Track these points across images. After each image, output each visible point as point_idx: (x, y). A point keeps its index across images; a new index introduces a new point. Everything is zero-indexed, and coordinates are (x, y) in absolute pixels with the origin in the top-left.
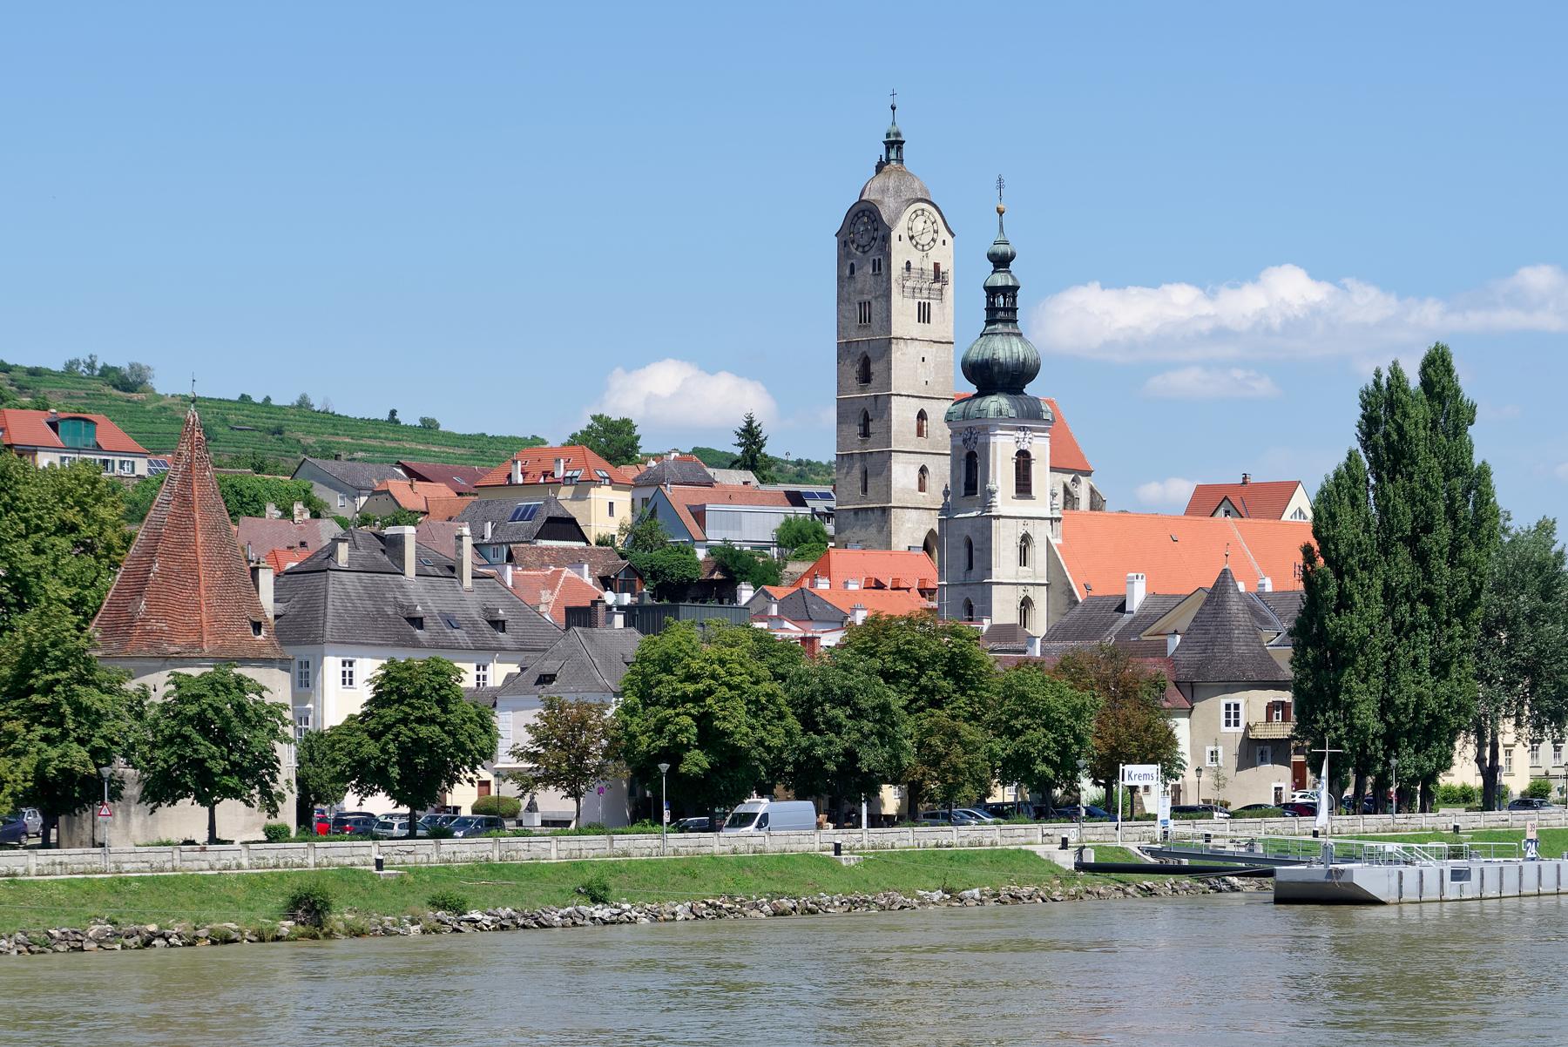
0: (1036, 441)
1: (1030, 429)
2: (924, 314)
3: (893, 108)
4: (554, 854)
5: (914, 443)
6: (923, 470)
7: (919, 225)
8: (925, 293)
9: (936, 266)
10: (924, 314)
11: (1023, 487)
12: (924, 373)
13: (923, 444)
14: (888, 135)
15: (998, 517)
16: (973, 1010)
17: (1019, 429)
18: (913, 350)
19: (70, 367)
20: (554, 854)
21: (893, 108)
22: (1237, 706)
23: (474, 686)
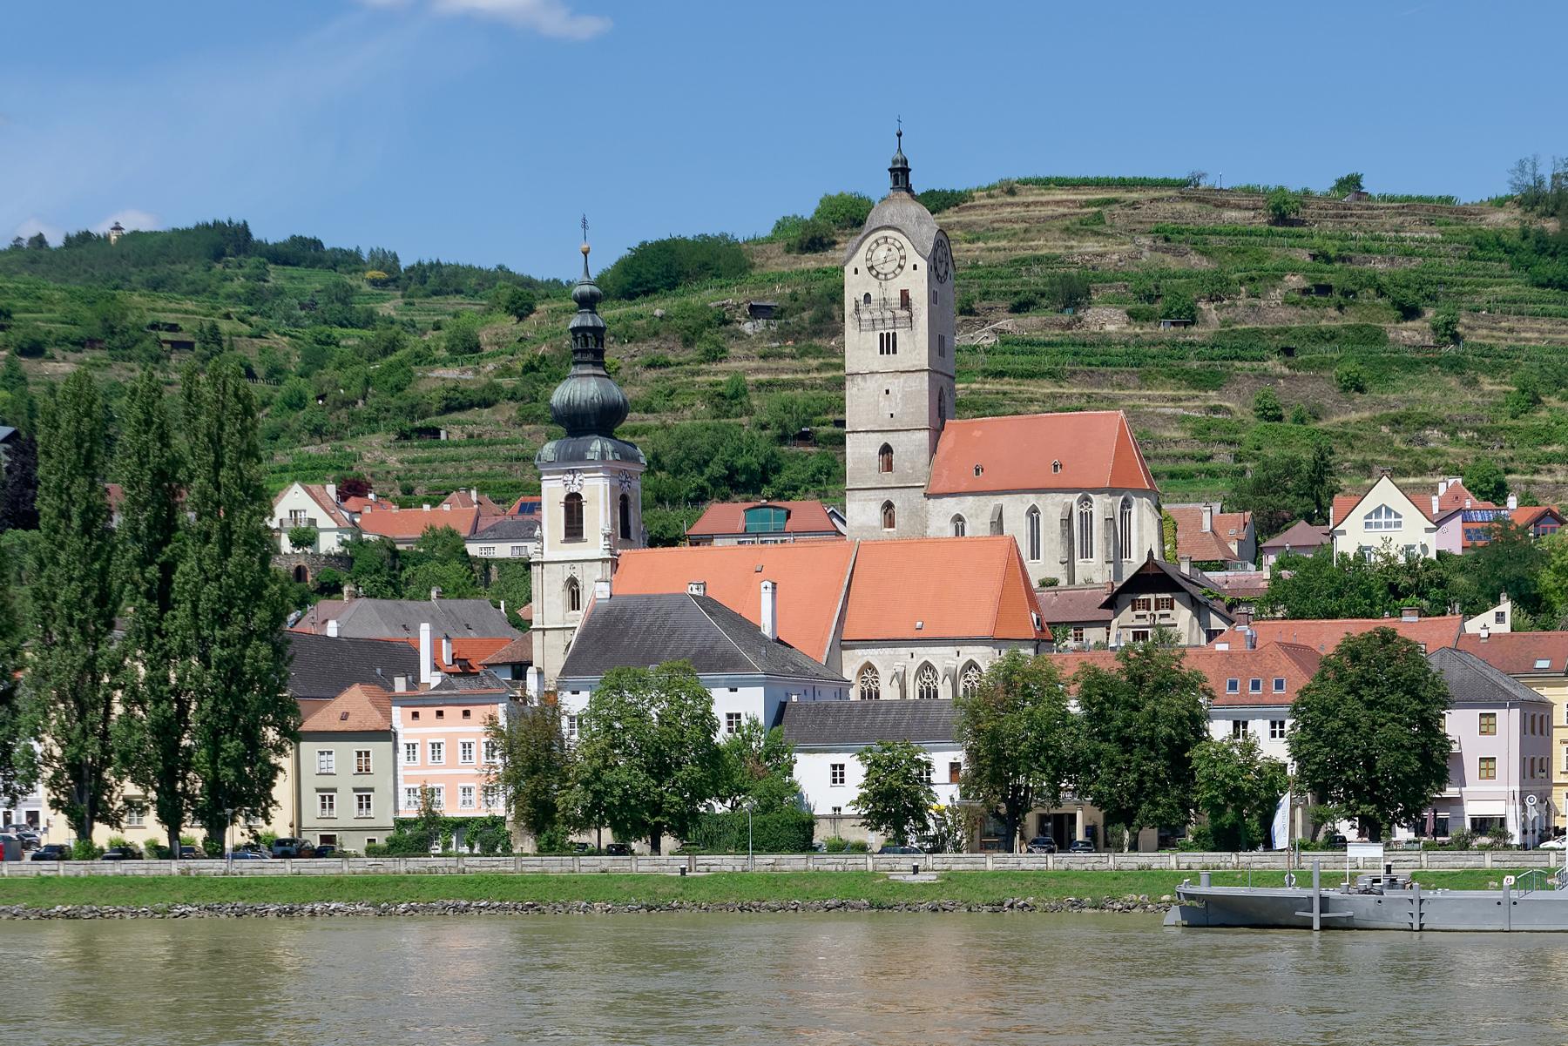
0: (587, 482)
1: (580, 471)
2: (888, 345)
3: (899, 135)
5: (874, 477)
6: (888, 506)
7: (881, 253)
9: (905, 295)
10: (888, 345)
11: (574, 529)
12: (886, 407)
13: (890, 479)
14: (895, 162)
15: (604, 560)
17: (568, 472)
18: (872, 384)
21: (899, 135)
22: (367, 754)
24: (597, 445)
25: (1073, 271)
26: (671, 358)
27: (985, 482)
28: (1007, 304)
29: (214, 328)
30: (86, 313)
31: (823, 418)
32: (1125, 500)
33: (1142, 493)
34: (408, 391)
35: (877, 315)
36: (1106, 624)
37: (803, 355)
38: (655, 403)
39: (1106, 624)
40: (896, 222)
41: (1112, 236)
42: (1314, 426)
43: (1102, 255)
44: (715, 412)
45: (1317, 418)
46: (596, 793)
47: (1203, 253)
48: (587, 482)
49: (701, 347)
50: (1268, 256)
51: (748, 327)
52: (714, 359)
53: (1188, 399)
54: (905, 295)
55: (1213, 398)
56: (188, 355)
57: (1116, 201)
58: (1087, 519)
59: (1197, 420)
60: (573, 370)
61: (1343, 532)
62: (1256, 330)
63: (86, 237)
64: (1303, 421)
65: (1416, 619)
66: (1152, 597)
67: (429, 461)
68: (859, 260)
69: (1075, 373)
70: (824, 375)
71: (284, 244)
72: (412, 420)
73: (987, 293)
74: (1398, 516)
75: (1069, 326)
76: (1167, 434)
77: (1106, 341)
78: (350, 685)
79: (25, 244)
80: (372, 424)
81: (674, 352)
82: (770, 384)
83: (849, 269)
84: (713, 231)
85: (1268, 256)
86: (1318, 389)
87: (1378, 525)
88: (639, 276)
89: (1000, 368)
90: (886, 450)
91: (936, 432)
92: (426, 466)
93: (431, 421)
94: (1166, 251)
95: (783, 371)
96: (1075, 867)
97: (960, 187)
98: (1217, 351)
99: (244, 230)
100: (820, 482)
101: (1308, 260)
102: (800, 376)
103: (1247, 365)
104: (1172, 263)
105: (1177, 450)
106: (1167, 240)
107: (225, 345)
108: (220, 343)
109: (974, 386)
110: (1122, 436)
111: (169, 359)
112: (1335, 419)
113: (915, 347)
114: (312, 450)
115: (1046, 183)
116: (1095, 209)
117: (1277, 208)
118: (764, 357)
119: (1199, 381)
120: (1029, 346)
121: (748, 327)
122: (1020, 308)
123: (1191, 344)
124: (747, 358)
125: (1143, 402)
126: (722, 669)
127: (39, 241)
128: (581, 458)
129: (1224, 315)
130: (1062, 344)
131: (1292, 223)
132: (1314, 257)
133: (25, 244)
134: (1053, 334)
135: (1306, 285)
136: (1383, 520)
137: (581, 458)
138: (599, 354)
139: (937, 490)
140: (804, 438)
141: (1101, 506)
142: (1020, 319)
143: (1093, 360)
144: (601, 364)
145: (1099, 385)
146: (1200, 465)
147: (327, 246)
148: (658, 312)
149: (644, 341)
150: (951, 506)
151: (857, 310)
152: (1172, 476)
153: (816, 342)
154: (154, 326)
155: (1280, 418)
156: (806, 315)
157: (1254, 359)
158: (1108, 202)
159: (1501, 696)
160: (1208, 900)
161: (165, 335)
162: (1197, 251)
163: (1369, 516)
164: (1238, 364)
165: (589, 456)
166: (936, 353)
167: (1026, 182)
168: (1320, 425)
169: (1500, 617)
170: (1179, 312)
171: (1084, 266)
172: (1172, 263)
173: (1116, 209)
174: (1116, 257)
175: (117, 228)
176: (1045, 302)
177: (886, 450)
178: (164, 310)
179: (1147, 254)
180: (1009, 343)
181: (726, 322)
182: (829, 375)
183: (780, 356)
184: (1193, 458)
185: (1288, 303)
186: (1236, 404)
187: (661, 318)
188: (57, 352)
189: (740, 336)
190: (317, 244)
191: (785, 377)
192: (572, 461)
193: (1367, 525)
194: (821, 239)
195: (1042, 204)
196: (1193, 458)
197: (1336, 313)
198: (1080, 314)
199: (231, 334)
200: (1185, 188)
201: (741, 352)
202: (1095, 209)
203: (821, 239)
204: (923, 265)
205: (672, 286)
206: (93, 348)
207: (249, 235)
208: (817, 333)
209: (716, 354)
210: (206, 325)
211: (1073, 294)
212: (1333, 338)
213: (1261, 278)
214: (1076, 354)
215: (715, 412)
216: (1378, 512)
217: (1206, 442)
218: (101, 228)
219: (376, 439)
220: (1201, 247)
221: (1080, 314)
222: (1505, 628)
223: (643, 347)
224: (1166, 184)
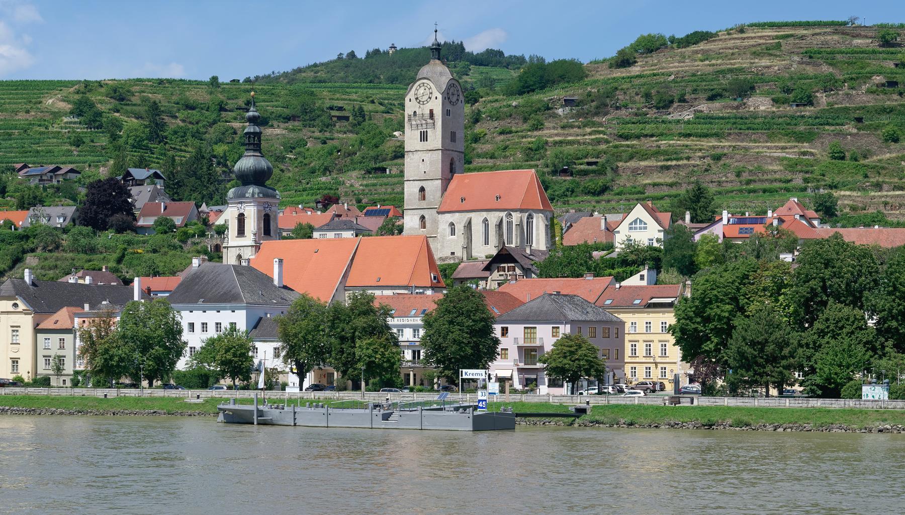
0: (247, 208)
2: (424, 137)
4: (787, 404)
6: (423, 218)
7: (421, 91)
8: (424, 126)
9: (431, 111)
10: (424, 137)
11: (241, 232)
13: (424, 204)
15: (252, 246)
16: (313, 462)
18: (417, 157)
19: (340, 58)
20: (787, 404)
23: (245, 311)
24: (251, 190)
25: (749, 77)
26: (514, 129)
27: (466, 205)
28: (706, 96)
29: (361, 110)
30: (295, 102)
31: (581, 161)
32: (530, 215)
33: (538, 211)
34: (381, 148)
35: (419, 122)
36: (486, 279)
37: (585, 126)
38: (496, 154)
39: (486, 279)
40: (429, 75)
41: (779, 56)
42: (862, 162)
43: (768, 67)
44: (526, 158)
45: (865, 157)
46: (106, 360)
47: (831, 64)
48: (247, 208)
49: (531, 122)
50: (869, 65)
51: (560, 111)
52: (536, 129)
53: (791, 148)
54: (431, 111)
55: (806, 147)
56: (346, 123)
57: (792, 36)
58: (510, 224)
59: (790, 159)
60: (246, 154)
61: (618, 232)
62: (846, 108)
63: (377, 52)
64: (856, 160)
65: (591, 278)
66: (506, 265)
67: (374, 185)
68: (411, 95)
69: (730, 134)
70: (593, 137)
71: (482, 54)
72: (376, 163)
73: (696, 90)
74: (645, 224)
75: (737, 108)
76: (771, 168)
77: (755, 116)
78: (62, 308)
79: (344, 56)
80: (353, 166)
81: (516, 125)
82: (561, 142)
83: (407, 99)
84: (568, 57)
85: (869, 65)
86: (868, 140)
87: (636, 228)
88: (526, 82)
89: (688, 132)
90: (422, 189)
91: (446, 182)
92: (372, 188)
93: (383, 164)
94: (808, 64)
95: (570, 135)
96: (273, 397)
97: (713, 31)
98: (817, 120)
99: (461, 47)
100: (566, 196)
101: (893, 66)
102: (579, 138)
103: (832, 128)
104: (810, 70)
105: (777, 176)
106: (811, 57)
107: (367, 118)
108: (364, 116)
109: (671, 142)
110: (531, 183)
111: (335, 125)
112: (875, 158)
113: (436, 138)
114: (323, 179)
115: (762, 26)
116: (777, 41)
117: (883, 37)
118: (563, 127)
119: (800, 138)
120: (710, 119)
121: (560, 111)
122: (711, 98)
123: (803, 117)
124: (554, 128)
125: (765, 150)
126: (230, 302)
127: (352, 55)
128: (243, 196)
129: (831, 100)
130: (729, 118)
131: (893, 45)
132: (897, 65)
133: (344, 56)
134: (725, 113)
135: (884, 81)
136: (638, 226)
137: (243, 196)
138: (259, 145)
139: (443, 210)
140: (564, 172)
141: (516, 217)
142: (717, 104)
143: (743, 127)
144: (259, 151)
145: (742, 141)
146: (783, 185)
147: (506, 55)
148: (514, 104)
149: (504, 119)
150: (449, 218)
151: (410, 120)
152: (765, 191)
153: (596, 119)
154: (331, 108)
155: (843, 158)
156: (594, 104)
157: (837, 124)
158: (788, 36)
159: (562, 318)
160: (235, 411)
161: (334, 113)
162: (827, 63)
163: (631, 224)
164: (827, 127)
165: (247, 195)
166: (448, 141)
167: (751, 25)
168: (866, 162)
169: (642, 278)
170: (801, 99)
171: (757, 74)
172: (810, 70)
173: (791, 40)
174: (776, 68)
175: (393, 47)
176: (727, 94)
177: (422, 189)
178: (337, 99)
179: (795, 66)
180: (701, 118)
181: (548, 109)
182: (593, 137)
183: (572, 127)
184: (780, 181)
185: (870, 92)
186: (818, 151)
187: (515, 107)
188: (275, 123)
189: (555, 116)
190: (501, 53)
191: (570, 138)
192: (240, 197)
193: (630, 228)
194: (628, 60)
195: (752, 38)
196: (780, 181)
197: (899, 97)
198: (745, 101)
199: (370, 112)
200: (838, 27)
201: (551, 125)
202: (777, 41)
203: (628, 60)
204: (440, 97)
205: (542, 88)
206: (294, 120)
207: (464, 49)
208: (597, 114)
209: (537, 127)
210: (357, 107)
211: (744, 89)
212: (891, 111)
213: (858, 78)
214: (735, 123)
215: (526, 158)
216: (635, 221)
217: (793, 172)
218: (384, 47)
219: (354, 174)
220: (829, 61)
221: (745, 101)
222: (644, 283)
223: (502, 123)
224: (832, 24)
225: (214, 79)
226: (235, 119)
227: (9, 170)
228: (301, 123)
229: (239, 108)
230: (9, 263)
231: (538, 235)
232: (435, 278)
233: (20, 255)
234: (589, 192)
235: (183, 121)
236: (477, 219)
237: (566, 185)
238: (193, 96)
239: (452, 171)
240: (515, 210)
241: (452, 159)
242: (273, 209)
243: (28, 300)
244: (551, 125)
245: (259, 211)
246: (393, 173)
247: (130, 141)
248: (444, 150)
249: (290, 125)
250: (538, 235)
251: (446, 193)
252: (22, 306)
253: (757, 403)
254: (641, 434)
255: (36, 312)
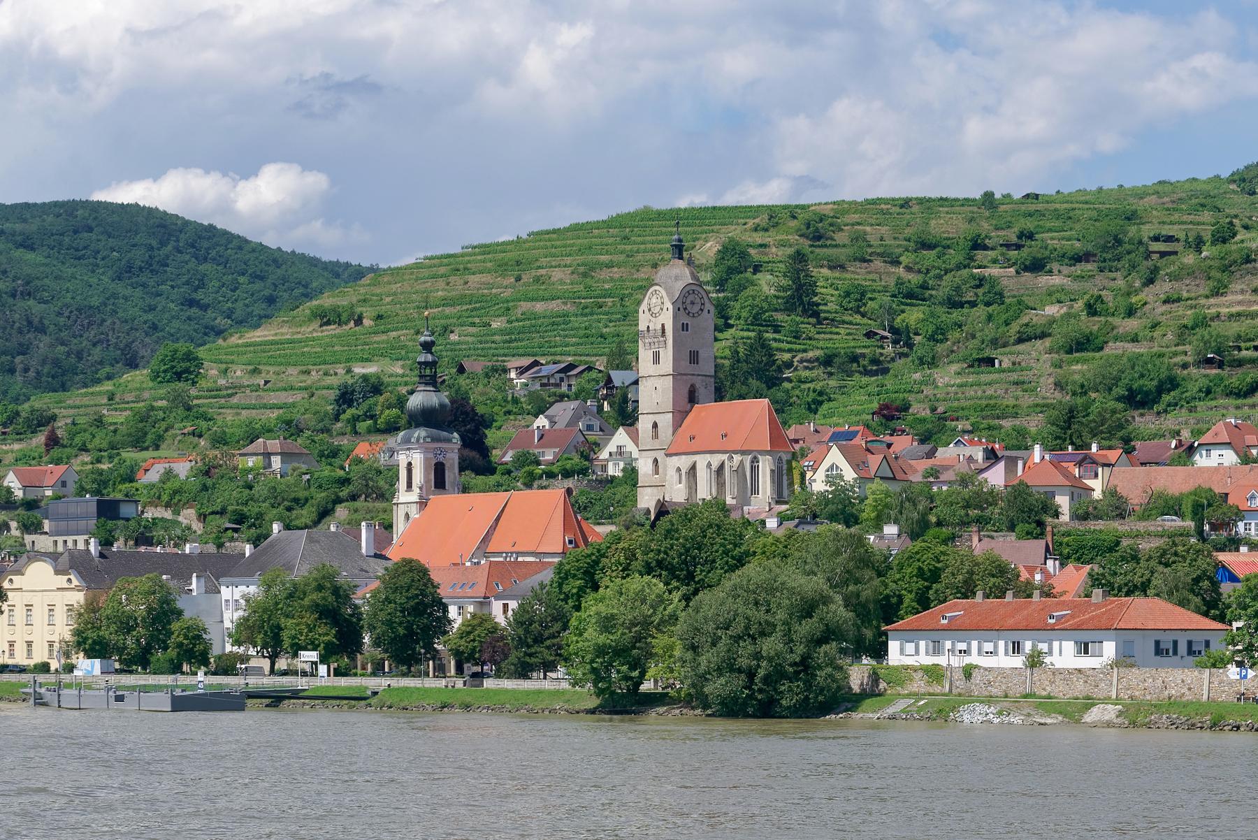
2: (656, 359)
10: (656, 359)
24: (421, 433)
27: (695, 445)
52: (1217, 294)
82: (1239, 314)
166: (685, 363)
188: (1055, 266)
204: (671, 307)
206: (1088, 261)
225: (989, 196)
226: (995, 261)
227: (496, 371)
228: (1095, 265)
229: (1008, 246)
230: (314, 516)
231: (765, 482)
232: (570, 542)
233: (330, 506)
234: (1231, 393)
235: (909, 269)
236: (702, 461)
237: (1203, 382)
238: (940, 227)
239: (692, 398)
240: (736, 452)
241: (692, 386)
242: (448, 455)
243: (82, 575)
244: (1239, 287)
245: (426, 459)
246: (1004, 365)
247: (744, 314)
248: (677, 375)
249: (1079, 268)
250: (765, 482)
251: (680, 430)
252: (75, 582)
253: (547, 685)
254: (691, 729)
255: (88, 588)
